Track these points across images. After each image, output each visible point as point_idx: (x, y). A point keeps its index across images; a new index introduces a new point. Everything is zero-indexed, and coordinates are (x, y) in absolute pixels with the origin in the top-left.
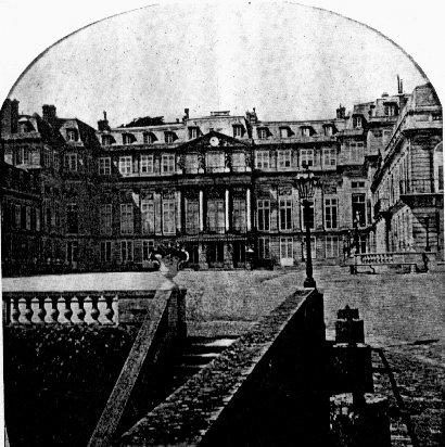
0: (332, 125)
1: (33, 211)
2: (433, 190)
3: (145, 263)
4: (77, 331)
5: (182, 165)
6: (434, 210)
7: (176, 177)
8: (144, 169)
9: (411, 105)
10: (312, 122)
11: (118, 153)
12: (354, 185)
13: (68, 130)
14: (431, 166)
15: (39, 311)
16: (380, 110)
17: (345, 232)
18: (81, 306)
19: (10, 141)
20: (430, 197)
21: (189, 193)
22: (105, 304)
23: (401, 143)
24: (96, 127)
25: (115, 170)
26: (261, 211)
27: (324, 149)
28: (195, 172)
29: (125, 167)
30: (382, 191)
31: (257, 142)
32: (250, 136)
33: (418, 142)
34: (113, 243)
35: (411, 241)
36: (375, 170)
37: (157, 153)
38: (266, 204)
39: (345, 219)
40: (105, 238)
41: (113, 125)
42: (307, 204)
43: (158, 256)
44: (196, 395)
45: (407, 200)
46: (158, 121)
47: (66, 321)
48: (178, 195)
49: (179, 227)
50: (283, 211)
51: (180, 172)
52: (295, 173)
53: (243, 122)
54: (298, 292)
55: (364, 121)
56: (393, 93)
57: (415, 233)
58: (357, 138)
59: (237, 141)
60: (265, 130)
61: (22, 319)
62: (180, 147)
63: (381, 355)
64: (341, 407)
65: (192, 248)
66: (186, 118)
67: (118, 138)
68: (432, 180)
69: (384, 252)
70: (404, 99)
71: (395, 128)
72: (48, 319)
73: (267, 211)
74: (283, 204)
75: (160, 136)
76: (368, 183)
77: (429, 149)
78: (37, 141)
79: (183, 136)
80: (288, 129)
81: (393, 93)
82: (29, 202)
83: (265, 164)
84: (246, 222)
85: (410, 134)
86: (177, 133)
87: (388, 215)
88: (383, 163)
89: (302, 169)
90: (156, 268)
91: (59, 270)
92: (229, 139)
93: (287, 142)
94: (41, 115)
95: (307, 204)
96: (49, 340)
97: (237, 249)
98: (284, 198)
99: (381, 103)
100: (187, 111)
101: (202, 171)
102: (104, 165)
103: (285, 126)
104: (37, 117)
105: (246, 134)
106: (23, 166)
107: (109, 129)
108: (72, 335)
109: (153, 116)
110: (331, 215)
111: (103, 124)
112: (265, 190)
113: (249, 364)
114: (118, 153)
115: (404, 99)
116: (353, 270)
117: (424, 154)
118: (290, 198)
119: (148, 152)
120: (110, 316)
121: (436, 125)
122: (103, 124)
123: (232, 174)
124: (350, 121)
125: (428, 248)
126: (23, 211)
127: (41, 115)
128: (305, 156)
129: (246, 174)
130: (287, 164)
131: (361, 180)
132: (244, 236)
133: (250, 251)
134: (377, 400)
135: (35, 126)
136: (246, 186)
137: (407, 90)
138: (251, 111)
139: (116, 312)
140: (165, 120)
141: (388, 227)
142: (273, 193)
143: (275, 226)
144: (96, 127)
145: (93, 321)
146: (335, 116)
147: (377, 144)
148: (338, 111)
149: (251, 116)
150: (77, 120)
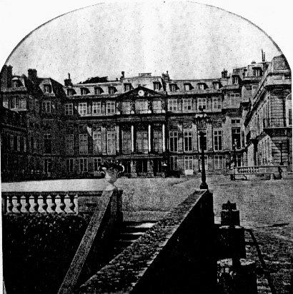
0: (219, 82)
1: (22, 139)
2: (285, 125)
3: (95, 173)
4: (51, 218)
5: (120, 109)
6: (286, 138)
7: (116, 116)
8: (95, 111)
9: (271, 69)
10: (206, 80)
11: (78, 101)
12: (233, 122)
13: (45, 86)
14: (284, 109)
15: (26, 204)
16: (250, 72)
17: (227, 153)
18: (53, 202)
19: (7, 93)
20: (283, 130)
21: (125, 127)
22: (69, 200)
23: (264, 94)
24: (63, 84)
25: (76, 111)
26: (172, 139)
27: (213, 98)
28: (129, 113)
29: (82, 110)
30: (252, 126)
31: (169, 94)
32: (165, 89)
33: (276, 94)
34: (74, 160)
35: (271, 159)
36: (247, 112)
37: (103, 100)
38: (175, 134)
39: (227, 144)
40: (69, 156)
41: (74, 82)
42: (202, 134)
43: (104, 168)
44: (129, 260)
45: (268, 132)
46: (104, 80)
47: (44, 211)
48: (117, 128)
49: (118, 149)
50: (186, 139)
51: (119, 113)
52: (195, 114)
53: (160, 80)
54: (196, 192)
55: (240, 80)
56: (259, 61)
57: (274, 153)
58: (235, 91)
59: (156, 93)
60: (174, 86)
61: (15, 210)
62: (118, 97)
63: (251, 233)
64: (224, 267)
65: (127, 163)
66: (122, 78)
67: (78, 91)
68: (285, 118)
69: (253, 166)
70: (266, 65)
71: (260, 84)
72: (32, 210)
73: (176, 139)
74: (186, 134)
75: (106, 90)
76: (243, 121)
77: (283, 98)
78: (24, 93)
79: (121, 89)
80: (190, 85)
81: (259, 61)
82: (19, 133)
83: (175, 108)
84: (162, 146)
85: (270, 88)
86: (117, 87)
87: (255, 142)
88: (252, 107)
89: (199, 111)
90: (103, 176)
91: (39, 178)
92: (151, 92)
93: (189, 93)
94: (27, 75)
95: (202, 134)
96: (32, 224)
97: (156, 164)
98: (187, 130)
99: (251, 68)
100: (123, 73)
101: (133, 112)
102: (69, 108)
103: (187, 83)
104: (24, 77)
105: (162, 88)
106: (15, 109)
107: (71, 85)
108: (48, 220)
109: (101, 76)
110: (218, 141)
111: (68, 82)
112: (174, 125)
113: (164, 240)
114: (78, 101)
115: (266, 65)
116: (233, 178)
117: (279, 101)
118: (191, 130)
119: (97, 100)
120: (72, 208)
121: (287, 82)
122: (68, 82)
123: (153, 114)
124: (231, 80)
125: (282, 163)
126: (15, 139)
127: (27, 75)
128: (201, 103)
129: (162, 114)
130: (189, 108)
131: (238, 118)
132: (161, 155)
133: (165, 165)
134: (248, 263)
135: (23, 83)
136: (162, 123)
137: (268, 59)
138: (165, 73)
139: (76, 205)
140: (109, 79)
141: (256, 150)
142: (180, 127)
143: (181, 148)
144: (63, 84)
145: (61, 211)
146: (220, 76)
147: (248, 95)
148: (222, 73)
149: (166, 76)
150: (50, 79)
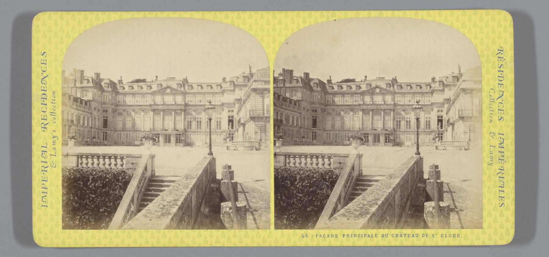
1: (298, 118)
2: (264, 114)
3: (136, 143)
4: (107, 172)
5: (363, 100)
6: (263, 123)
7: (360, 105)
8: (137, 102)
9: (255, 78)
10: (212, 83)
11: (335, 94)
13: (314, 83)
14: (263, 104)
15: (92, 162)
16: (451, 79)
17: (433, 131)
18: (110, 161)
19: (289, 87)
20: (262, 118)
22: (327, 159)
23: (460, 93)
24: (326, 82)
25: (334, 101)
26: (188, 121)
27: (426, 95)
28: (369, 103)
29: (338, 100)
30: (242, 114)
31: (187, 91)
32: (184, 89)
33: (258, 93)
34: (331, 133)
35: (254, 136)
36: (447, 105)
37: (353, 94)
38: (400, 118)
39: (434, 125)
40: (128, 131)
41: (333, 82)
42: (418, 119)
43: (351, 139)
44: (165, 200)
45: (252, 118)
46: (353, 81)
47: (310, 166)
48: (361, 113)
49: (361, 127)
50: (407, 121)
51: (362, 103)
52: (413, 105)
53: (390, 82)
54: (412, 157)
55: (234, 83)
56: (247, 72)
57: (256, 133)
58: (231, 91)
59: (387, 90)
61: (314, 166)
63: (448, 186)
64: (226, 207)
65: (366, 135)
66: (366, 80)
67: (126, 87)
68: (263, 110)
69: (242, 140)
70: (252, 75)
71: (457, 87)
72: (95, 165)
73: (400, 121)
74: (407, 118)
75: (145, 87)
76: (236, 110)
77: (263, 98)
78: (301, 87)
79: (364, 88)
81: (456, 72)
82: (296, 114)
83: (400, 101)
84: (390, 125)
85: (255, 90)
86: (361, 86)
87: (244, 125)
88: (242, 102)
89: (416, 103)
90: (350, 144)
91: (296, 144)
92: (176, 90)
94: (303, 76)
95: (418, 119)
96: (303, 174)
98: (408, 116)
99: (451, 76)
101: (371, 103)
102: (329, 97)
103: (410, 85)
104: (301, 78)
105: (392, 88)
106: (295, 98)
107: (331, 83)
108: (105, 173)
109: (142, 79)
110: (428, 124)
111: (329, 81)
112: (399, 112)
113: (390, 188)
114: (335, 94)
115: (252, 75)
116: (437, 148)
117: (261, 100)
118: (410, 116)
119: (349, 93)
120: (330, 165)
121: (266, 86)
122: (329, 81)
123: (155, 104)
124: (228, 83)
125: (261, 140)
126: (293, 117)
127: (303, 76)
128: (418, 98)
129: (391, 105)
130: (410, 101)
131: (232, 109)
132: (389, 131)
133: (392, 139)
135: (300, 81)
136: (181, 110)
137: (253, 71)
138: (185, 78)
139: (332, 163)
140: (147, 80)
141: (244, 130)
142: (194, 113)
143: (403, 128)
144: (326, 82)
145: (322, 167)
146: (430, 81)
147: (449, 93)
